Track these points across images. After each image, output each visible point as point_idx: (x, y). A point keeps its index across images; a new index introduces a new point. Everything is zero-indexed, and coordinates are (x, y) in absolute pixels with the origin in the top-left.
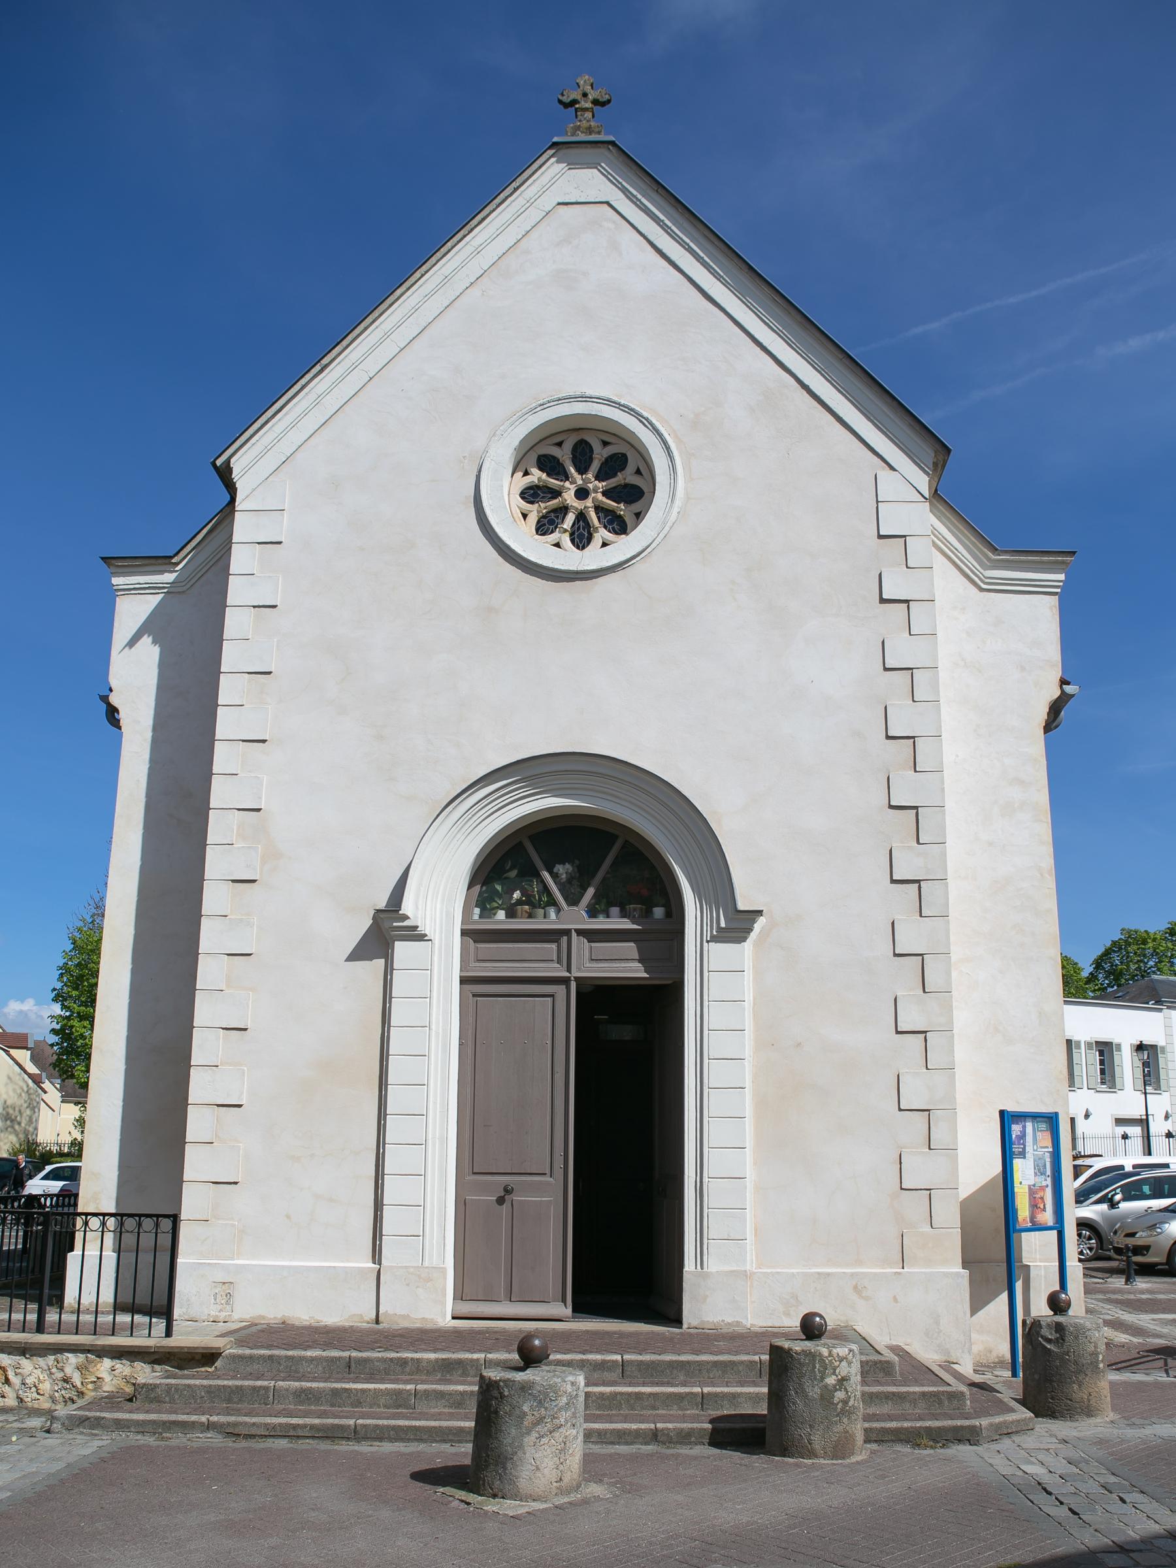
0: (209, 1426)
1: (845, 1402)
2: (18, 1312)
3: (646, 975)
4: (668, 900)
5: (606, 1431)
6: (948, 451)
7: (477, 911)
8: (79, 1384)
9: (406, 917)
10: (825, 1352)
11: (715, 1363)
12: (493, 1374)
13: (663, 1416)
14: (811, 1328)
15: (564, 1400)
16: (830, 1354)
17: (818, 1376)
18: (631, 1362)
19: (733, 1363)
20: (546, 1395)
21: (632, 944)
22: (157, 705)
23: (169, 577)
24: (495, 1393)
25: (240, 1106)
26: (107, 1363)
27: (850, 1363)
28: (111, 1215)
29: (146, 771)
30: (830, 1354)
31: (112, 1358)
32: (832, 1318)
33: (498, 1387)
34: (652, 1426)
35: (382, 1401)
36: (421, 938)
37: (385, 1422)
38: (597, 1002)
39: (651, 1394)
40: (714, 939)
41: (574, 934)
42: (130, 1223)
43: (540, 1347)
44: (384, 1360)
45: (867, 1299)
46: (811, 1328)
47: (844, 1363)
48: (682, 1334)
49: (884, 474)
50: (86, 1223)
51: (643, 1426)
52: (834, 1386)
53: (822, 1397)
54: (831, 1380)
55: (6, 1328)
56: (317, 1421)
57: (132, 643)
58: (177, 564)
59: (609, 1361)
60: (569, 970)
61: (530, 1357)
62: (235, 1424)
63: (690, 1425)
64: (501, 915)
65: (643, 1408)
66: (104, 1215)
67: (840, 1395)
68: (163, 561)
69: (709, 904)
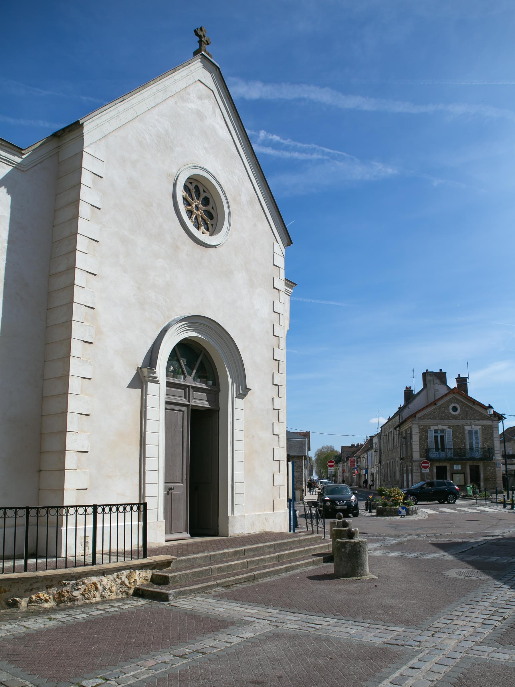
0: (217, 585)
3: (210, 407)
6: (292, 243)
8: (128, 584)
21: (205, 394)
22: (10, 229)
23: (18, 160)
24: (358, 546)
25: (87, 452)
26: (138, 572)
28: (135, 504)
29: (4, 265)
31: (139, 570)
40: (238, 397)
45: (267, 522)
49: (276, 243)
55: (2, 572)
58: (24, 154)
60: (189, 401)
62: (225, 582)
68: (18, 150)
69: (236, 383)
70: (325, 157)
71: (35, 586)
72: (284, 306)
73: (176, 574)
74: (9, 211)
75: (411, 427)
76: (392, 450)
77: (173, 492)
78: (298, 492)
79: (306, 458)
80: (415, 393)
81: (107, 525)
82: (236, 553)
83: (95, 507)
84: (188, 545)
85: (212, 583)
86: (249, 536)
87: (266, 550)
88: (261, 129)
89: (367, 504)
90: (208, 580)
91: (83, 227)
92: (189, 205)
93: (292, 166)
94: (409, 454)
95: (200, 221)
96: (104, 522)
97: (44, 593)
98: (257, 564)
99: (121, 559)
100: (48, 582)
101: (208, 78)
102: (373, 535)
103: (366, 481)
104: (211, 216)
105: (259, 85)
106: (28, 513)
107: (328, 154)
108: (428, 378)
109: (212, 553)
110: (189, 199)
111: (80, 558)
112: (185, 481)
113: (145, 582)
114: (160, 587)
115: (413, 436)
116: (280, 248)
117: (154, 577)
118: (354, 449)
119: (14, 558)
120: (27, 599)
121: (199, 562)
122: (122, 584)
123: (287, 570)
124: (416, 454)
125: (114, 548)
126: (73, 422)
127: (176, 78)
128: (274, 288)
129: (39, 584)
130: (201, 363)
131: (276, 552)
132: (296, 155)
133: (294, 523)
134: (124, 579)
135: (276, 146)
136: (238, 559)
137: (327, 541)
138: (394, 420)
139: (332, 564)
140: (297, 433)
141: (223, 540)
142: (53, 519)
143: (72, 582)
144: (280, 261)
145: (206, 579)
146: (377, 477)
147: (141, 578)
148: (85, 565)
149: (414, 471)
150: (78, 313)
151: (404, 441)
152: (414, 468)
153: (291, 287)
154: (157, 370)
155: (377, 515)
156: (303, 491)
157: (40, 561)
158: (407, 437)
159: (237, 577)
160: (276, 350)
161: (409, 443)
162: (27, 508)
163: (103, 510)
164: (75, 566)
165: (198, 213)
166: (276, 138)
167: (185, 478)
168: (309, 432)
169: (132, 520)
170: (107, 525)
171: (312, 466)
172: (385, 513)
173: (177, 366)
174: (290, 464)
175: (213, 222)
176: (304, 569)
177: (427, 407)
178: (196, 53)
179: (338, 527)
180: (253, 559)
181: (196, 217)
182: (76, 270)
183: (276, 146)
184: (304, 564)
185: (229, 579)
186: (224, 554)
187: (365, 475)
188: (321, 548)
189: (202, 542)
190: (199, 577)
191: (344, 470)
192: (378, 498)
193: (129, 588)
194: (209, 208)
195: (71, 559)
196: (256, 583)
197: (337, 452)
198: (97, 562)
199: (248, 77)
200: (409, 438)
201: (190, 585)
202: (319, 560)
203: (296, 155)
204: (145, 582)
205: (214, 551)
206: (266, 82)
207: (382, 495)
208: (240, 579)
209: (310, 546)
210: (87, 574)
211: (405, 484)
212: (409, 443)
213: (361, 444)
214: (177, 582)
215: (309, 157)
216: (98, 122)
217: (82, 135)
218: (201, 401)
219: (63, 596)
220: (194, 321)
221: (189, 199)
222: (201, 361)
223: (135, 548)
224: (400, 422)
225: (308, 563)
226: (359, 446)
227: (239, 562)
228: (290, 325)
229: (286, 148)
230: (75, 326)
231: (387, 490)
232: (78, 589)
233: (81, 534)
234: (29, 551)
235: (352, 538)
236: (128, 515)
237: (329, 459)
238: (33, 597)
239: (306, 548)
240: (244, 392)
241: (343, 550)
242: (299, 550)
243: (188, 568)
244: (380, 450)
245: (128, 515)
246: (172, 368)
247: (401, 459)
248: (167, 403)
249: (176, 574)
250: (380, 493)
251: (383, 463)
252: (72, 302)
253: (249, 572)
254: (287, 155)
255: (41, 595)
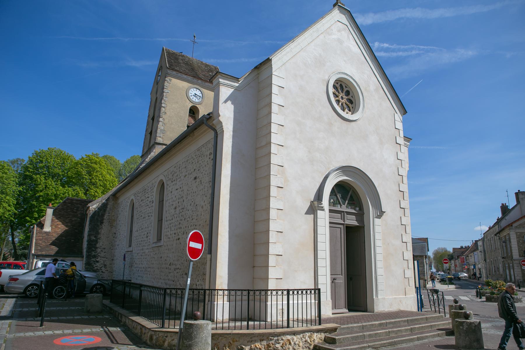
0: (369, 347)
2: (177, 325)
23: (237, 85)
26: (315, 334)
38: (349, 229)
40: (376, 217)
42: (233, 293)
49: (395, 114)
50: (272, 293)
57: (226, 102)
60: (344, 221)
62: (374, 345)
66: (224, 290)
68: (237, 79)
70: (421, 52)
71: (254, 339)
72: (404, 154)
73: (341, 337)
74: (233, 113)
75: (509, 234)
76: (494, 251)
77: (336, 281)
78: (422, 281)
79: (426, 256)
80: (510, 207)
81: (296, 302)
82: (380, 325)
83: (288, 291)
84: (347, 317)
85: (365, 345)
86: (389, 313)
87: (402, 324)
88: (376, 41)
89: (477, 292)
90: (363, 343)
91: (274, 118)
92: (337, 97)
93: (399, 61)
94: (510, 255)
95: (344, 105)
96: (294, 300)
97: (259, 344)
98: (396, 334)
99: (305, 325)
100: (261, 337)
101: (343, 18)
102: (485, 317)
103: (475, 274)
104: (351, 102)
105: (371, 15)
106: (249, 293)
107: (423, 49)
108: (521, 196)
109: (364, 324)
110: (337, 93)
111: (280, 323)
112: (343, 274)
113: (321, 341)
114: (330, 345)
115: (512, 241)
116: (398, 117)
117: (326, 338)
118: (462, 250)
119: (241, 320)
120: (249, 347)
121: (355, 329)
122: (305, 341)
123: (418, 339)
124: (516, 254)
125: (300, 317)
126: (273, 237)
127: (324, 22)
128: (397, 143)
129: (256, 338)
130: (351, 196)
131: (409, 326)
132: (401, 54)
133: (421, 305)
134: (307, 338)
135: (386, 50)
136: (382, 329)
137: (447, 319)
138: (494, 228)
139: (453, 337)
140: (418, 239)
141: (371, 315)
142: (263, 298)
143: (275, 338)
144: (400, 125)
145: (361, 342)
146: (484, 271)
147: (318, 338)
148: (282, 328)
149: (515, 267)
150: (274, 170)
151: (504, 244)
152: (515, 265)
153: (408, 141)
154: (323, 202)
155: (486, 301)
156: (425, 280)
157: (256, 323)
158: (506, 242)
159: (382, 342)
160: (401, 184)
161: (508, 246)
162: (248, 290)
163: (293, 293)
164: (277, 328)
165: (343, 101)
166: (386, 45)
167: (343, 272)
168: (427, 238)
169: (311, 299)
170: (296, 302)
171: (431, 262)
172: (493, 300)
173: (335, 199)
174: (416, 262)
175: (353, 105)
176: (431, 339)
177: (521, 218)
178: (334, 5)
179: (456, 309)
180: (393, 330)
181: (342, 104)
182: (272, 145)
183: (386, 50)
184: (431, 336)
185: (377, 343)
186: (373, 325)
187: (473, 269)
188: (444, 324)
189: (356, 316)
190: (356, 340)
191: (456, 266)
192: (485, 287)
193: (311, 345)
194: (350, 97)
195: (274, 323)
196: (396, 347)
197: (449, 252)
198: (290, 326)
199: (364, 12)
200: (508, 242)
201: (350, 345)
202: (442, 334)
203: (401, 54)
204: (321, 341)
205: (365, 322)
206: (375, 12)
207: (489, 285)
208: (385, 343)
209: (434, 322)
210: (284, 334)
211: (508, 277)
212: (508, 246)
213: (469, 246)
214: (341, 342)
215: (409, 53)
216: (280, 56)
217: (271, 65)
218: (352, 221)
219: (270, 347)
220: (345, 169)
221: (337, 93)
222: (351, 195)
223: (313, 318)
224: (499, 230)
225: (434, 335)
226: (467, 248)
227: (383, 331)
228: (409, 167)
229: (393, 51)
230: (272, 178)
231: (493, 282)
232: (279, 343)
233: (280, 307)
234: (250, 317)
235: (468, 319)
236: (309, 296)
237: (444, 258)
238: (252, 346)
239: (432, 324)
240: (380, 214)
241: (461, 327)
242: (427, 325)
243: (348, 334)
244: (484, 251)
245: (309, 296)
246: (332, 200)
247: (503, 258)
248: (330, 223)
249: (341, 337)
250: (488, 284)
251: (488, 261)
252: (270, 163)
253: (391, 339)
254: (394, 54)
255: (257, 345)
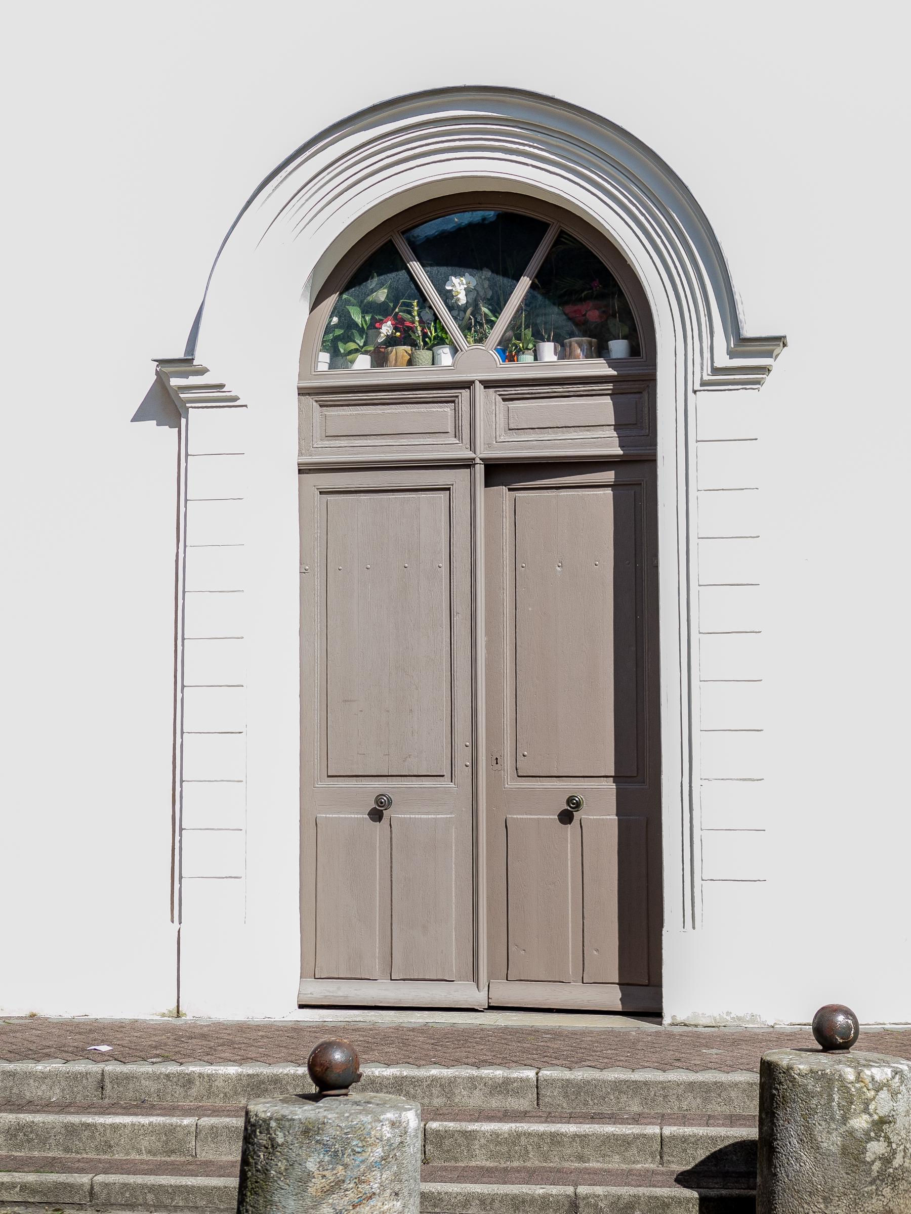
1: (886, 1161)
4: (633, 329)
5: (493, 1198)
7: (325, 357)
9: (202, 371)
10: (850, 1074)
11: (691, 1086)
12: (262, 1108)
13: (595, 1172)
14: (831, 1034)
15: (379, 1151)
16: (859, 1079)
17: (838, 1115)
18: (551, 1082)
19: (720, 1086)
20: (346, 1143)
27: (894, 1094)
30: (859, 1079)
32: (872, 1014)
33: (268, 1128)
34: (570, 1190)
35: (144, 1143)
36: (231, 401)
37: (139, 1179)
39: (575, 1136)
41: (478, 385)
43: (342, 1063)
44: (156, 1077)
46: (831, 1034)
47: (884, 1094)
48: (657, 1033)
51: (554, 1190)
52: (867, 1133)
53: (845, 1151)
54: (860, 1123)
56: (31, 1178)
59: (515, 1080)
60: (472, 447)
61: (328, 1081)
63: (633, 1191)
64: (363, 362)
65: (562, 1158)
67: (876, 1148)
